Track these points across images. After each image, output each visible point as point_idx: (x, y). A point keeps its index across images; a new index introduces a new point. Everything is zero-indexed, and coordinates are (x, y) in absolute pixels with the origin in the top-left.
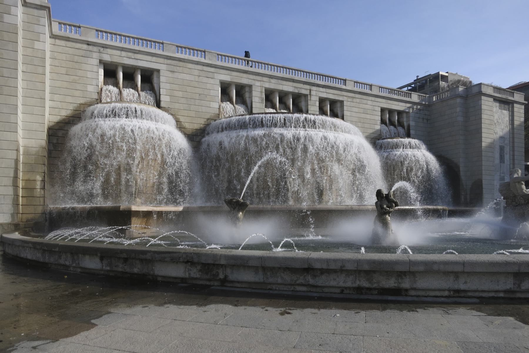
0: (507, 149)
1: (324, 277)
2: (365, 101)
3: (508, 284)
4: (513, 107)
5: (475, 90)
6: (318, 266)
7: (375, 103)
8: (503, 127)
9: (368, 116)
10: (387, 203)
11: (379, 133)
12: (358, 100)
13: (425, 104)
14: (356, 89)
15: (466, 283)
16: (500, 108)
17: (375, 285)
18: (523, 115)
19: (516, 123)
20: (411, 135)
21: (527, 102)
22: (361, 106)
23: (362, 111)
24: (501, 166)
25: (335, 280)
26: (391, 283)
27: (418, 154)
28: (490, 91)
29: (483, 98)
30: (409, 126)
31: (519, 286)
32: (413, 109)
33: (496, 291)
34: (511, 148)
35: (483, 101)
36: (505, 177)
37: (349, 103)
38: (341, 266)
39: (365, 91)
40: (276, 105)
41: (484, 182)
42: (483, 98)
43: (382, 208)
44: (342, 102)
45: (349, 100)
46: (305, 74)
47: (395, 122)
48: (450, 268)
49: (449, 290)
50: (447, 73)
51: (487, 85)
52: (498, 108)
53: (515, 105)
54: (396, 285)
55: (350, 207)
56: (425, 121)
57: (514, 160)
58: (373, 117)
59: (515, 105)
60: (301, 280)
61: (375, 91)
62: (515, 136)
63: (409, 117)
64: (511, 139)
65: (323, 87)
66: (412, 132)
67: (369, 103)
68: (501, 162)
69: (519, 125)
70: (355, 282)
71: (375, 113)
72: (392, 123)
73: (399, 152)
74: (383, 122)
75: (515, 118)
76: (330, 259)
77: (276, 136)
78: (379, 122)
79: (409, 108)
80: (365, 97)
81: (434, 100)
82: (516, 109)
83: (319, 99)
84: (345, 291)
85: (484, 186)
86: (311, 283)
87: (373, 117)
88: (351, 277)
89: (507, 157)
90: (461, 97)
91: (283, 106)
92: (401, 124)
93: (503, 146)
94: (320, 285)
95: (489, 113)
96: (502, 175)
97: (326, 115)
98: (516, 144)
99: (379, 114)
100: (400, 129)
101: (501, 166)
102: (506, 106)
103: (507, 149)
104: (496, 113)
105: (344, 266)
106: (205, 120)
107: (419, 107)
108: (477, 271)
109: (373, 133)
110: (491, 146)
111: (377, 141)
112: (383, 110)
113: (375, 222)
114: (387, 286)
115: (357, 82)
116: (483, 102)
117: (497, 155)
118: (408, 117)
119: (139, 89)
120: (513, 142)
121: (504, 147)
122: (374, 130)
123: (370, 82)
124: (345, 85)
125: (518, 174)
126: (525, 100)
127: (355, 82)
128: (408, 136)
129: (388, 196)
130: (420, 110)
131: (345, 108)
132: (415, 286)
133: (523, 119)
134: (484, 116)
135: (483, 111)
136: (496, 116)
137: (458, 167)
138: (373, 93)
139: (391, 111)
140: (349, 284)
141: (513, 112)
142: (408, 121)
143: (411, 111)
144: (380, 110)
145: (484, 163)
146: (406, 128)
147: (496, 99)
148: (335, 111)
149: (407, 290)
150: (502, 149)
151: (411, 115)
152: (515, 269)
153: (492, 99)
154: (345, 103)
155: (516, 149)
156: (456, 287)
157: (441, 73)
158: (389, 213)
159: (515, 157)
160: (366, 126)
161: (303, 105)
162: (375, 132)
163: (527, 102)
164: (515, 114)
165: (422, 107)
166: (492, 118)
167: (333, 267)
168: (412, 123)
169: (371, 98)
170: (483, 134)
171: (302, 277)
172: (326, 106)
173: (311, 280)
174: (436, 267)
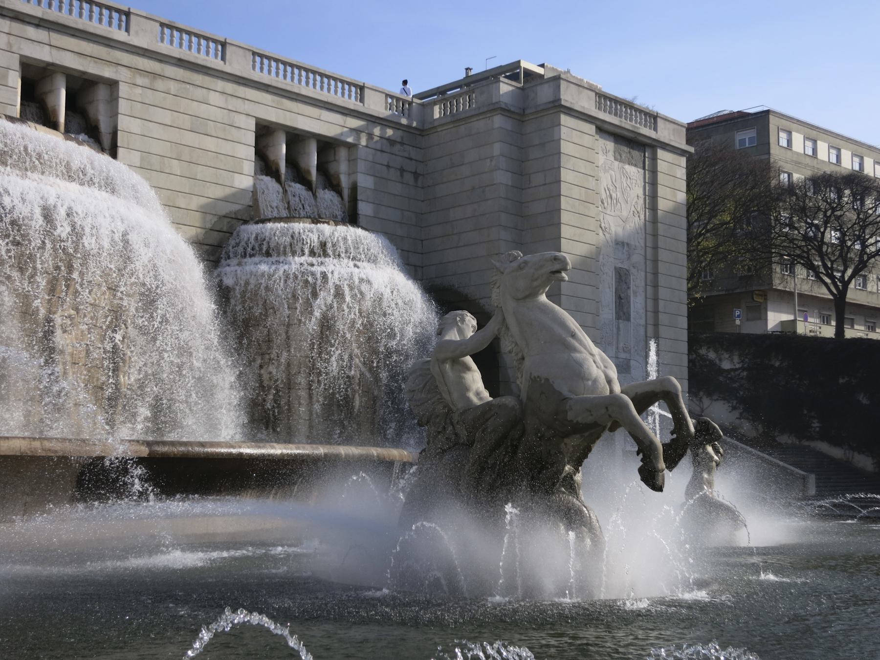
0: (638, 280)
2: (199, 93)
4: (654, 159)
5: (544, 95)
7: (234, 104)
8: (625, 214)
9: (210, 143)
11: (248, 201)
12: (173, 86)
13: (409, 127)
14: (164, 48)
16: (618, 157)
18: (683, 185)
19: (663, 205)
20: (361, 220)
21: (692, 149)
22: (184, 105)
23: (186, 122)
24: (618, 329)
27: (370, 281)
28: (586, 104)
29: (565, 119)
30: (354, 188)
32: (370, 136)
34: (650, 276)
35: (563, 130)
36: (632, 363)
37: (139, 90)
39: (197, 61)
40: (55, 113)
42: (565, 119)
44: (113, 85)
45: (139, 80)
46: (303, 73)
47: (309, 172)
50: (542, 66)
51: (579, 85)
52: (611, 155)
53: (661, 153)
56: (409, 178)
57: (656, 312)
58: (227, 148)
59: (661, 153)
61: (239, 64)
62: (660, 244)
63: (355, 160)
65: (37, 26)
66: (364, 209)
67: (215, 98)
68: (618, 318)
69: (673, 213)
71: (235, 134)
72: (299, 175)
74: (265, 164)
75: (661, 191)
77: (22, 210)
78: (249, 166)
79: (357, 131)
80: (198, 78)
81: (437, 115)
82: (661, 166)
83: (257, 125)
87: (227, 148)
89: (637, 303)
90: (505, 111)
91: (33, 108)
92: (331, 182)
93: (625, 270)
95: (582, 166)
96: (623, 355)
97: (53, 125)
98: (662, 268)
99: (251, 139)
100: (327, 196)
101: (618, 329)
102: (636, 154)
103: (638, 280)
104: (605, 171)
106: (215, 219)
107: (390, 132)
109: (225, 200)
110: (589, 264)
112: (264, 131)
115: (171, 27)
116: (564, 132)
117: (608, 296)
118: (352, 161)
119: (283, 177)
120: (655, 261)
121: (627, 273)
122: (228, 191)
123: (360, 80)
124: (127, 30)
125: (461, 332)
126: (689, 142)
127: (162, 25)
128: (352, 218)
130: (391, 141)
131: (123, 106)
133: (682, 197)
134: (566, 175)
135: (563, 159)
136: (605, 181)
138: (227, 68)
139: (296, 138)
141: (654, 172)
142: (352, 172)
143: (363, 142)
144: (253, 128)
146: (346, 193)
147: (603, 129)
148: (332, 168)
150: (622, 277)
151: (362, 153)
153: (591, 128)
154: (123, 90)
157: (524, 64)
159: (661, 304)
160: (201, 172)
161: (100, 113)
162: (234, 195)
163: (692, 149)
164: (660, 177)
165: (400, 133)
166: (591, 183)
168: (365, 182)
169: (220, 85)
170: (564, 229)
172: (54, 91)
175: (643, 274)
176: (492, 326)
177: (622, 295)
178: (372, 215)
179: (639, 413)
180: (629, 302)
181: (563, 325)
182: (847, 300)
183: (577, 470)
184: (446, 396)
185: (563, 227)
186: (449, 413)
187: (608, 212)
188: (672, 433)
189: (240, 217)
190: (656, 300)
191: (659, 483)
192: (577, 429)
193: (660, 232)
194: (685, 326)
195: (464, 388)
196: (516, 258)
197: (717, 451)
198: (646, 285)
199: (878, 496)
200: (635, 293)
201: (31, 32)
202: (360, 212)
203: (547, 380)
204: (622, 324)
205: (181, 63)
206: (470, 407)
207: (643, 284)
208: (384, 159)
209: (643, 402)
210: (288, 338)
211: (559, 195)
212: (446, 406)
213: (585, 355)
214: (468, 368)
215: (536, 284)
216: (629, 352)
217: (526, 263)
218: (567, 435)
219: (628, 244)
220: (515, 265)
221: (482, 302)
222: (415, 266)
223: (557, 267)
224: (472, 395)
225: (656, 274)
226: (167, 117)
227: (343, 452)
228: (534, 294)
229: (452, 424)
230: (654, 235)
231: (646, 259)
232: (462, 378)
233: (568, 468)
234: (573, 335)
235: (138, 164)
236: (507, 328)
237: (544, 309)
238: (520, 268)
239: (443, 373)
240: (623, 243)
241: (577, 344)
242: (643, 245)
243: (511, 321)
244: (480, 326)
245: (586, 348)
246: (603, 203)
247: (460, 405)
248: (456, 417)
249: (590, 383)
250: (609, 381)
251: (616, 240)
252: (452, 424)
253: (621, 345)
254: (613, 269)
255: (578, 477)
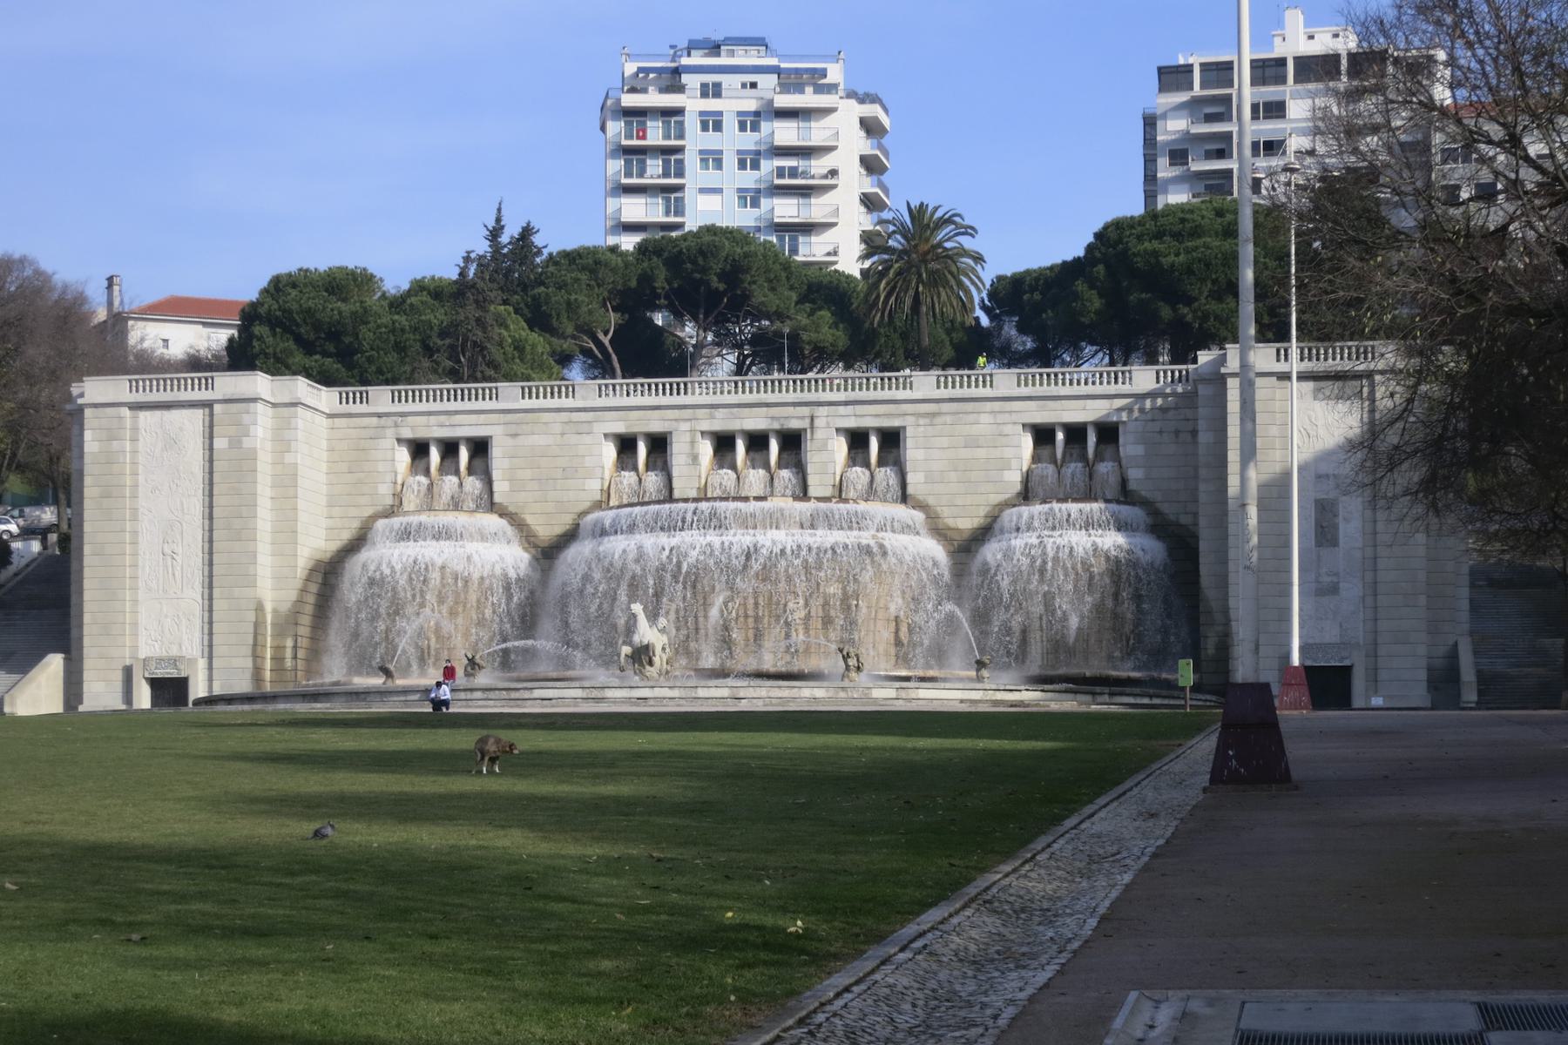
2: (972, 418)
7: (1001, 418)
12: (948, 419)
45: (922, 421)
68: (1319, 544)
80: (970, 406)
130: (1163, 410)
169: (989, 406)
182: (60, 710)
201: (841, 409)
205: (846, 403)
208: (1157, 426)
226: (945, 442)
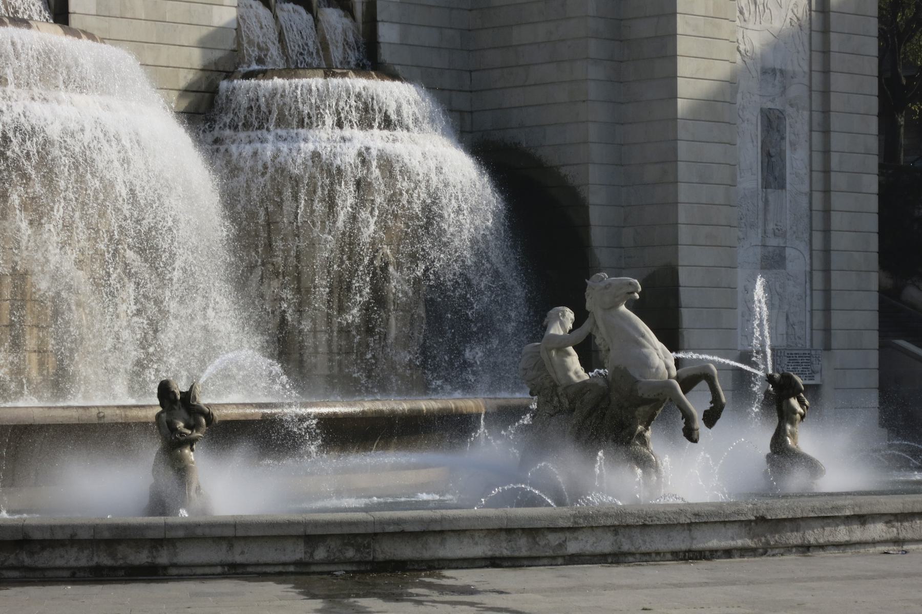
0: (798, 126)
1: (46, 554)
3: (296, 552)
6: (37, 536)
10: (186, 416)
11: (230, 45)
15: (242, 553)
17: (121, 562)
24: (766, 202)
25: (62, 557)
26: (142, 558)
31: (312, 555)
33: (284, 564)
34: (817, 117)
36: (789, 252)
38: (71, 536)
41: (684, 277)
43: (173, 429)
48: (218, 532)
49: (222, 565)
54: (149, 560)
55: (94, 412)
57: (827, 171)
60: (12, 560)
64: (817, 78)
68: (766, 185)
70: (92, 559)
73: (321, 139)
76: (55, 526)
84: (78, 574)
85: (685, 296)
86: (26, 564)
88: (86, 552)
89: (797, 161)
94: (40, 566)
96: (773, 242)
98: (836, 102)
101: (766, 202)
103: (798, 126)
105: (76, 535)
108: (252, 534)
110: (720, 104)
111: (224, 85)
113: (155, 465)
114: (137, 563)
117: (749, 153)
125: (562, 325)
128: (371, 61)
129: (188, 397)
132: (175, 561)
137: (582, 207)
140: (83, 562)
145: (684, 193)
149: (165, 568)
150: (772, 123)
152: (301, 531)
155: (836, 122)
156: (229, 559)
158: (191, 442)
159: (835, 159)
167: (59, 536)
171: (12, 556)
173: (26, 559)
174: (199, 532)
175: (806, 114)
176: (586, 327)
177: (773, 151)
178: (397, 41)
179: (685, 393)
180: (783, 160)
181: (636, 329)
183: (647, 429)
184: (553, 375)
185: (680, 60)
186: (555, 386)
187: (750, 25)
188: (711, 403)
189: (221, 69)
190: (826, 152)
191: (696, 437)
192: (645, 402)
193: (834, 46)
194: (875, 188)
195: (566, 369)
196: (603, 279)
197: (802, 403)
198: (811, 131)
199: (920, 446)
200: (792, 144)
202: (381, 40)
203: (625, 368)
204: (772, 195)
206: (571, 384)
207: (806, 128)
209: (688, 384)
210: (412, 324)
211: (674, 14)
212: (552, 381)
213: (652, 350)
214: (569, 354)
215: (617, 300)
216: (784, 235)
217: (610, 284)
218: (639, 406)
219: (781, 71)
220: (602, 285)
221: (563, 171)
222: (461, 112)
223: (631, 289)
224: (572, 374)
225: (826, 112)
227: (424, 408)
228: (617, 305)
229: (558, 396)
230: (824, 52)
231: (811, 90)
232: (564, 361)
233: (640, 428)
234: (643, 336)
235: (94, 12)
236: (597, 328)
237: (624, 317)
238: (606, 288)
239: (550, 358)
240: (774, 71)
241: (646, 343)
242: (806, 69)
243: (600, 323)
244: (577, 324)
245: (652, 345)
246: (741, 13)
247: (563, 382)
248: (560, 390)
249: (654, 370)
250: (668, 368)
251: (762, 68)
252: (558, 396)
253: (771, 226)
254: (757, 112)
255: (648, 434)
